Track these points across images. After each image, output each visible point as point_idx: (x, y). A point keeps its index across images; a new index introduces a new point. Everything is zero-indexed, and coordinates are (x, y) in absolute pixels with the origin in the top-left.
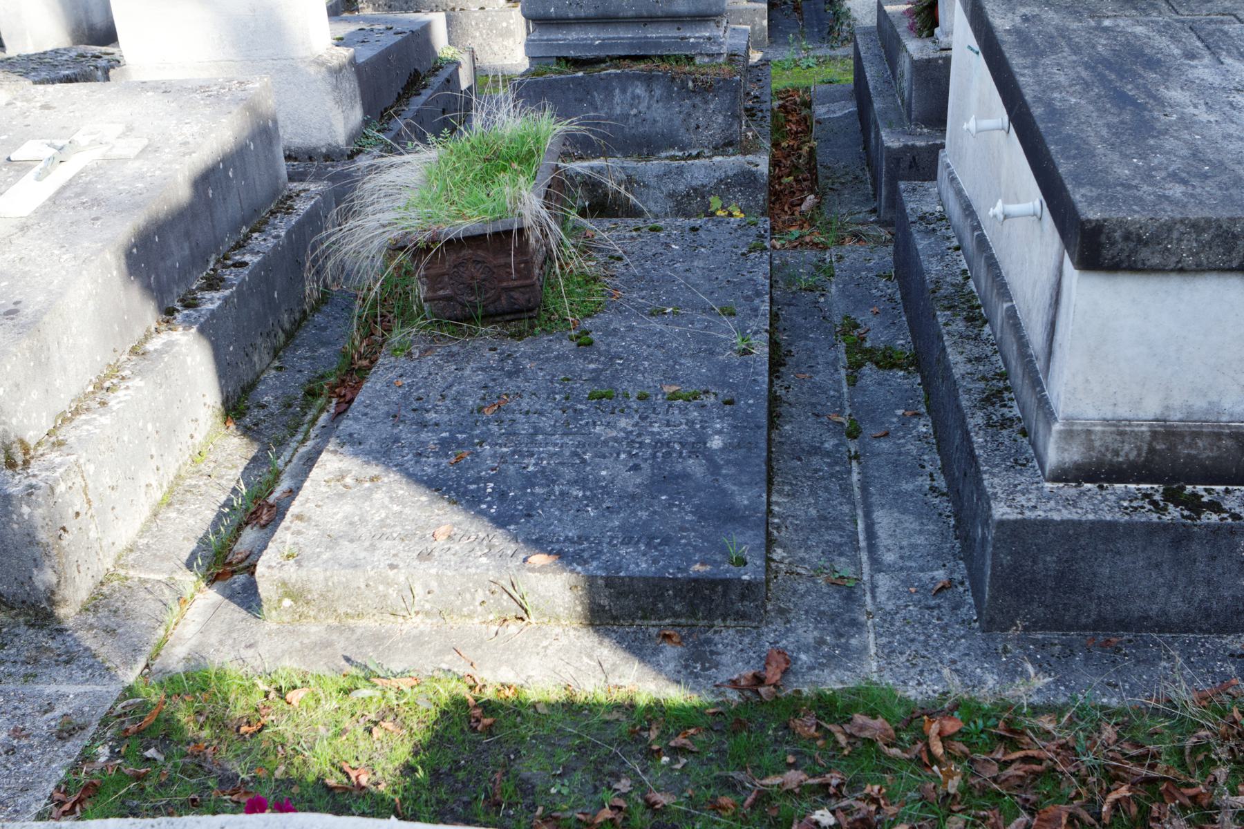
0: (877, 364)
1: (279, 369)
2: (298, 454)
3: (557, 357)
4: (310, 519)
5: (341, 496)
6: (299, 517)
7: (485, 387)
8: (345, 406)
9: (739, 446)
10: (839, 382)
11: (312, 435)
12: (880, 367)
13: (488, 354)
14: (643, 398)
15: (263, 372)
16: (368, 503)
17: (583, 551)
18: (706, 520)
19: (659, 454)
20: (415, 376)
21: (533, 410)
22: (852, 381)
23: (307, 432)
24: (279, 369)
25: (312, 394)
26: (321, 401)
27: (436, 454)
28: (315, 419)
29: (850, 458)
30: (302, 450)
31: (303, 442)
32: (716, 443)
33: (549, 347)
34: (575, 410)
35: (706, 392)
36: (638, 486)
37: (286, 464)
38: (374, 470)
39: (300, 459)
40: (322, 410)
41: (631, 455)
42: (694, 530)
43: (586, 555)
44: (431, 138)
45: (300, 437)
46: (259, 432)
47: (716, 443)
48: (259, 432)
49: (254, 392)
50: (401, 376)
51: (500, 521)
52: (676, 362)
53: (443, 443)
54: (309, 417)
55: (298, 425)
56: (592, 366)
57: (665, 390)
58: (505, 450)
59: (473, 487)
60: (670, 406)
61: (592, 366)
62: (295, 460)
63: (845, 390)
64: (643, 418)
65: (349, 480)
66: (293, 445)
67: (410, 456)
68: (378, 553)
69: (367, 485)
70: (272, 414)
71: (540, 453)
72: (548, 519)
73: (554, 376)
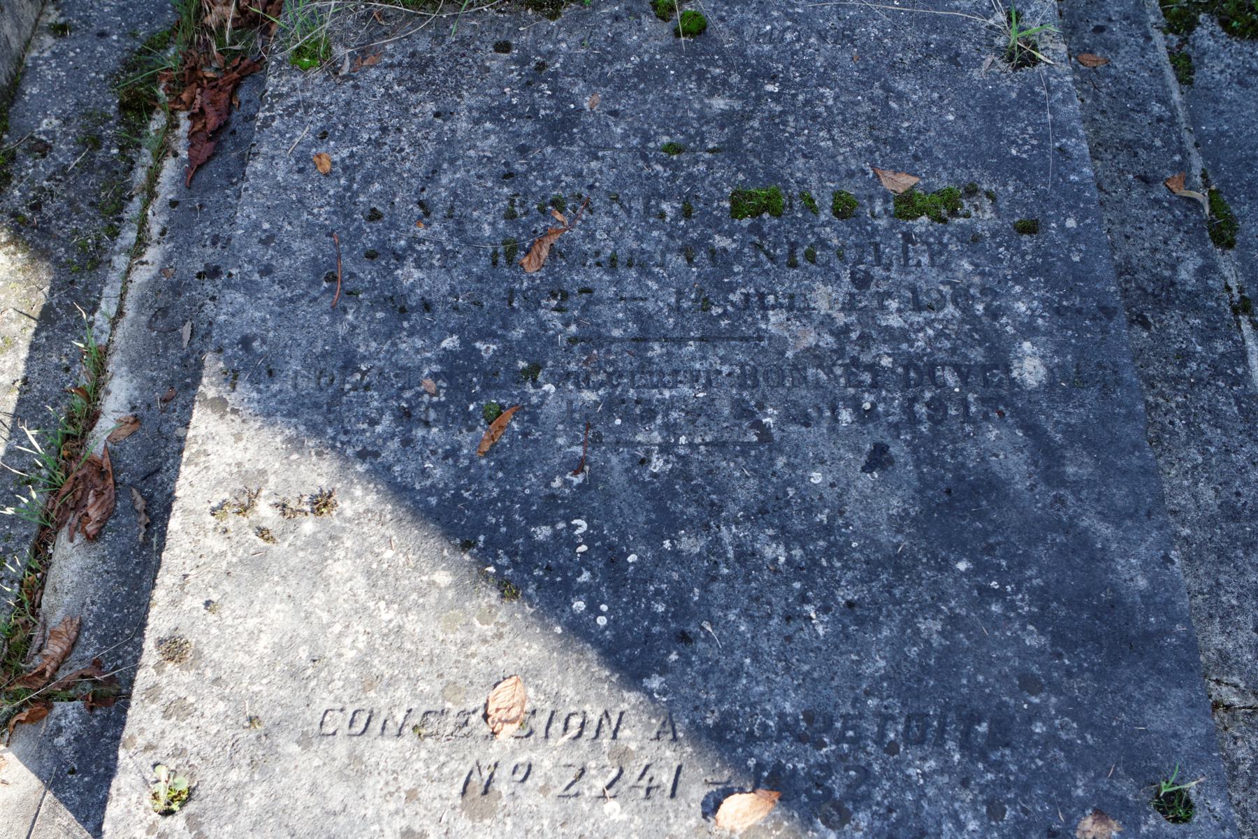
0: (1225, 24)
1: (59, 30)
2: (133, 292)
3: (641, 72)
4: (199, 654)
5: (257, 565)
6: (174, 649)
7: (508, 176)
8: (208, 147)
9: (1081, 380)
10: (1157, 72)
11: (155, 230)
12: (1232, 32)
13: (496, 63)
14: (844, 209)
15: (27, 44)
16: (320, 597)
17: (827, 768)
18: (1071, 646)
19: (921, 410)
20: (355, 140)
21: (623, 255)
22: (1185, 67)
23: (143, 222)
24: (59, 30)
25: (137, 107)
26: (157, 122)
27: (447, 421)
28: (153, 177)
29: (1235, 311)
30: (141, 276)
31: (142, 243)
32: (1030, 367)
33: (615, 40)
34: (713, 253)
35: (971, 191)
36: (898, 523)
37: (114, 323)
38: (317, 472)
39: (141, 303)
40: (163, 151)
41: (865, 417)
42: (1056, 689)
43: (837, 785)
44: (704, 740)
45: (129, 236)
46: (45, 232)
47: (1030, 367)
48: (45, 232)
49: (18, 104)
50: (324, 135)
51: (628, 659)
52: (887, 88)
53: (455, 370)
54: (140, 175)
55: (121, 201)
56: (719, 103)
57: (887, 184)
58: (589, 396)
59: (543, 533)
60: (907, 237)
61: (719, 103)
62: (130, 313)
63: (1176, 97)
64: (862, 282)
65: (265, 511)
66: (121, 261)
67: (387, 420)
68: (374, 785)
69: (309, 526)
70: (63, 169)
71: (669, 406)
72: (729, 650)
73: (646, 138)
